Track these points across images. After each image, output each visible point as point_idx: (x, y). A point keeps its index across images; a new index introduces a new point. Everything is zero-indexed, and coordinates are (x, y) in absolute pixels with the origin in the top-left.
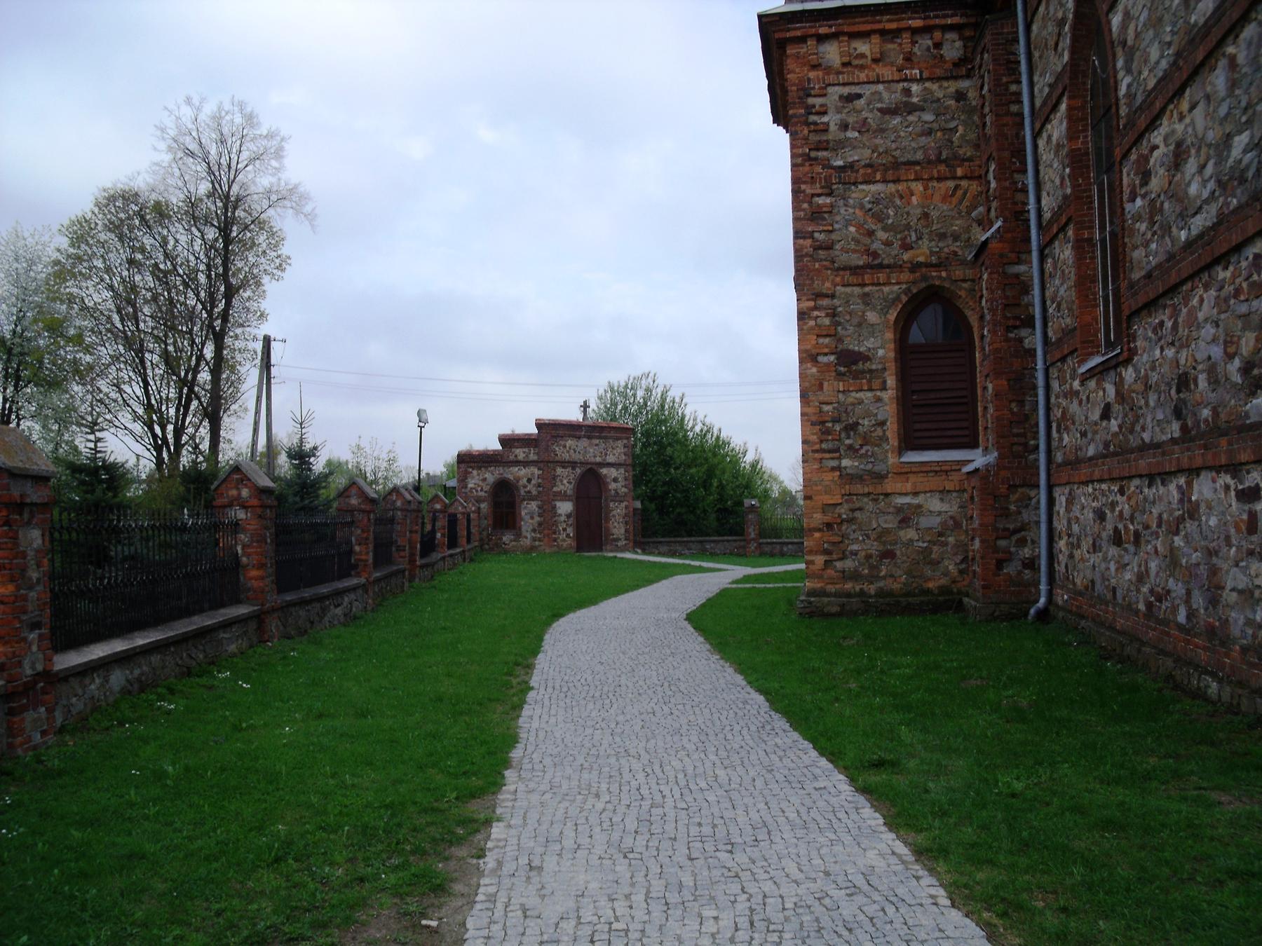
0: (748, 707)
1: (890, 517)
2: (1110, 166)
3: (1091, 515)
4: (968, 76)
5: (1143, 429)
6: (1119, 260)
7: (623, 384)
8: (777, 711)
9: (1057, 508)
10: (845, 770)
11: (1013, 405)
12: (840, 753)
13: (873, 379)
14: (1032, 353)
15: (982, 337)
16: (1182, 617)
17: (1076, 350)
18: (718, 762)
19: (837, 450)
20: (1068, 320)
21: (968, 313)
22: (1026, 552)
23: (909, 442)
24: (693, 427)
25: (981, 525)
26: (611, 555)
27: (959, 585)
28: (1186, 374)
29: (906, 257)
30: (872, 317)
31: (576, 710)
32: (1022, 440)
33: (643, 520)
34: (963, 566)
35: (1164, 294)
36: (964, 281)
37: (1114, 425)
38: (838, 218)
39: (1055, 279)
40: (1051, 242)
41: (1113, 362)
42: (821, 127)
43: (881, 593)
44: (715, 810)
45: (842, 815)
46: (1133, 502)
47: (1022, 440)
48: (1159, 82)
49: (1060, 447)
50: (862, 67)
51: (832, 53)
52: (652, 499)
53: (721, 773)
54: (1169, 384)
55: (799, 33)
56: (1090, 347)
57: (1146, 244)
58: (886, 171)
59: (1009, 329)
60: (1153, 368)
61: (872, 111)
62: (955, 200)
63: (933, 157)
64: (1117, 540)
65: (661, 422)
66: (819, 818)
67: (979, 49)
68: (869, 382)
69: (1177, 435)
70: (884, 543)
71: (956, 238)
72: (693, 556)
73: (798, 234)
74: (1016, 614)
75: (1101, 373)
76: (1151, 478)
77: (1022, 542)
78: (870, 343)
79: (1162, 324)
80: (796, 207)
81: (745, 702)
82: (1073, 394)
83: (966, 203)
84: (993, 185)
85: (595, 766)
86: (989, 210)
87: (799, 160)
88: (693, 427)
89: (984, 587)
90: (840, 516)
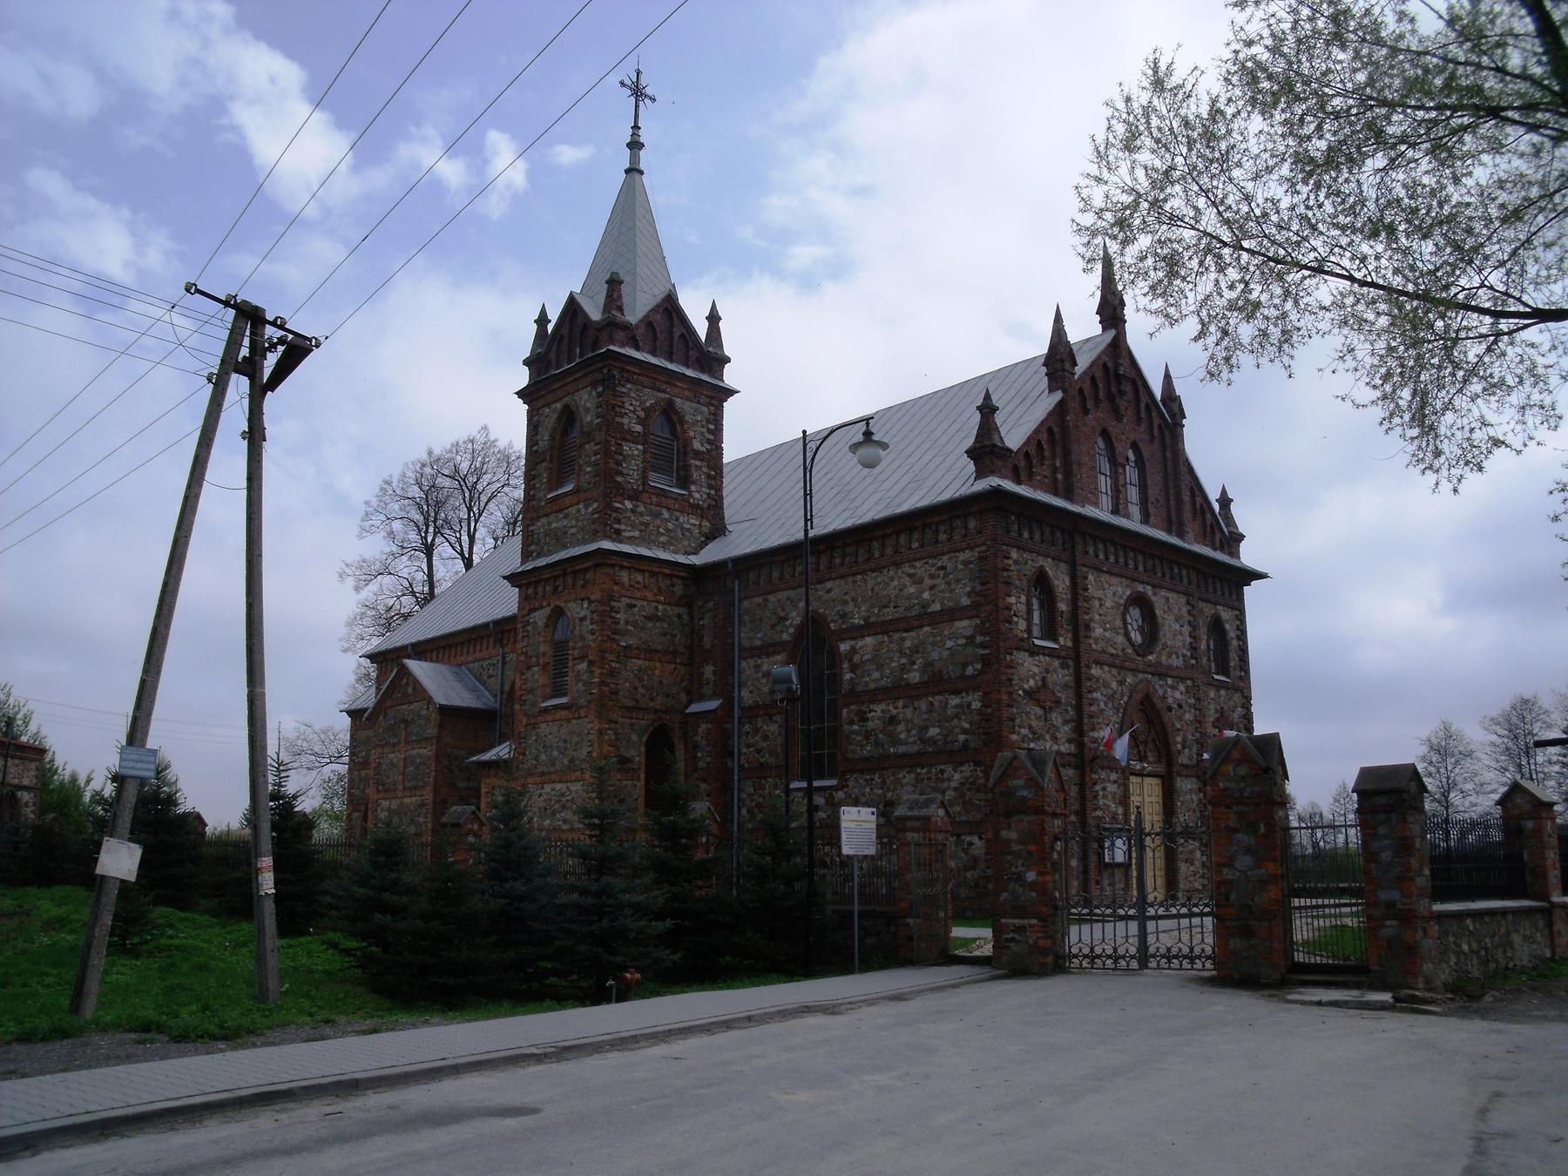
30: (634, 737)
51: (624, 576)
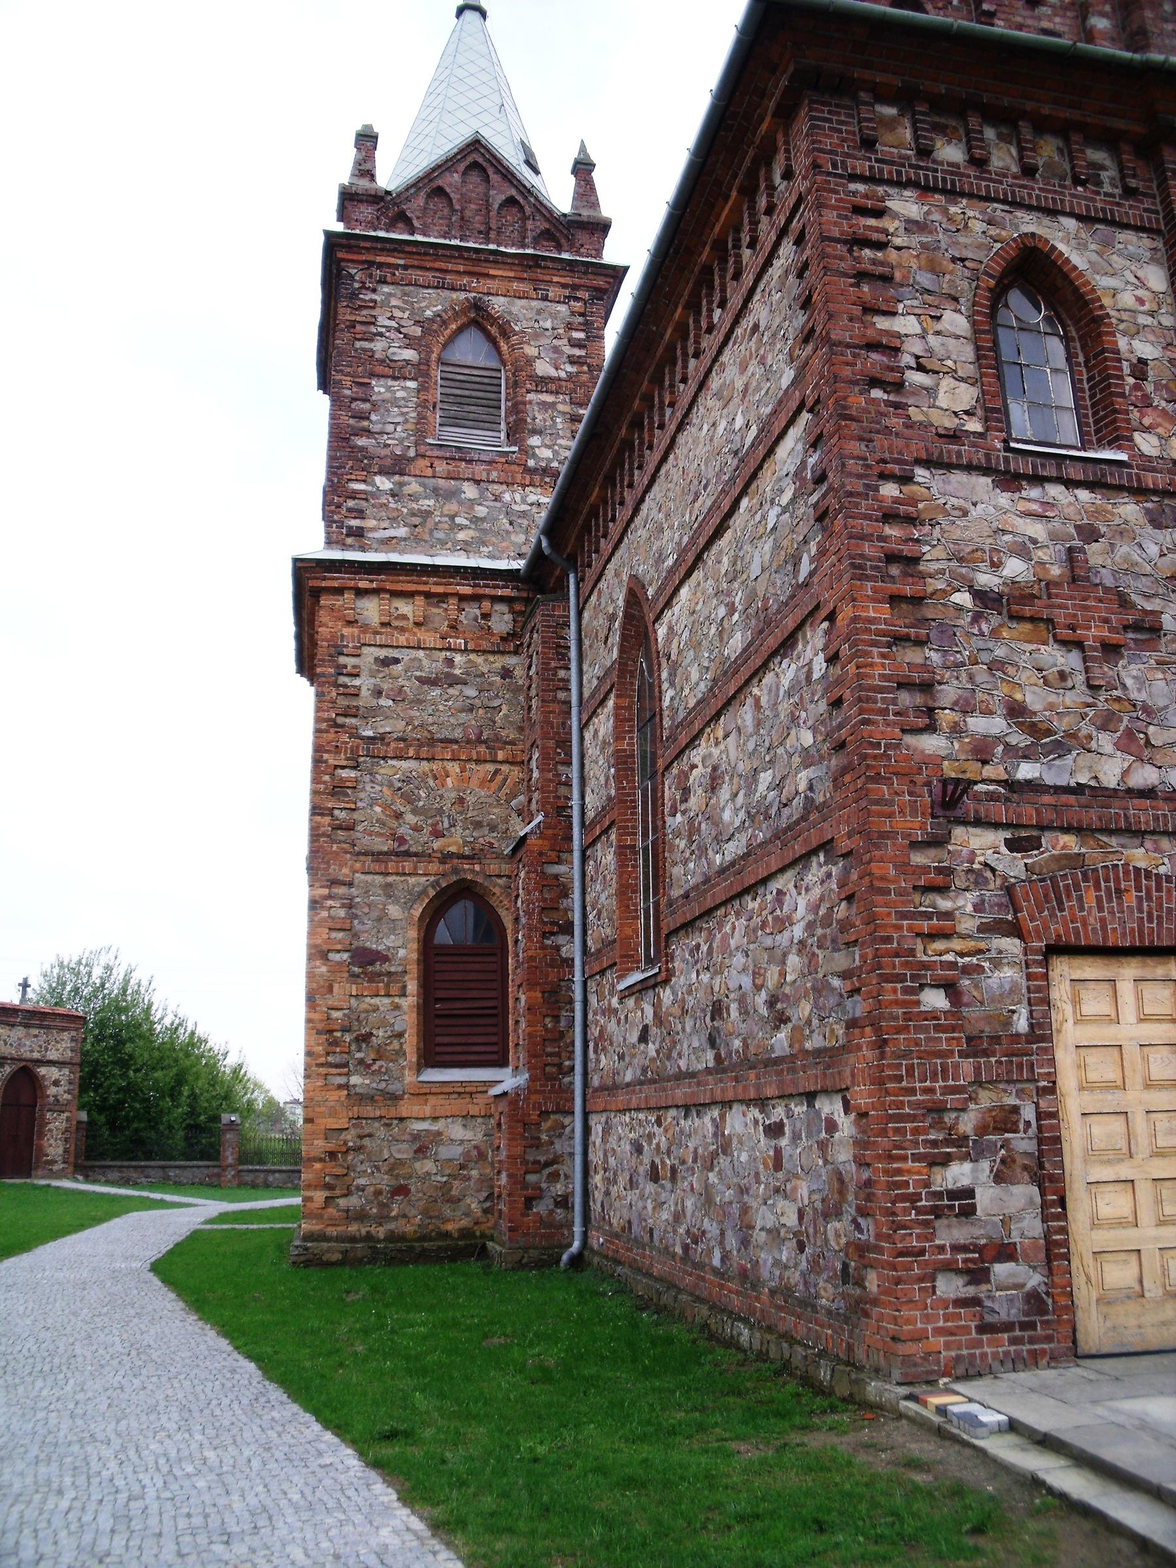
0: (237, 1377)
1: (405, 1146)
2: (654, 775)
3: (628, 1147)
4: (516, 652)
5: (680, 1055)
6: (659, 876)
7: (75, 959)
8: (271, 1380)
9: (592, 1138)
10: (353, 1443)
11: (548, 1020)
12: (347, 1424)
13: (391, 982)
14: (569, 962)
15: (516, 941)
16: (716, 1261)
17: (615, 964)
18: (206, 1442)
19: (346, 1065)
20: (608, 931)
21: (502, 913)
22: (559, 1188)
23: (430, 1057)
24: (162, 1019)
25: (508, 1157)
26: (43, 1182)
27: (483, 1227)
28: (720, 1001)
29: (437, 845)
30: (394, 911)
31: (21, 1389)
32: (556, 1060)
33: (87, 1137)
34: (488, 1204)
35: (701, 916)
36: (499, 876)
37: (652, 1049)
38: (362, 795)
39: (596, 885)
40: (593, 843)
41: (652, 982)
42: (352, 691)
43: (392, 1237)
44: (207, 1498)
45: (351, 1492)
46: (669, 1135)
47: (556, 1060)
48: (699, 703)
49: (598, 1069)
50: (402, 630)
51: (371, 610)
52: (101, 1109)
53: (210, 1455)
54: (704, 1011)
55: (336, 584)
56: (628, 962)
57: (685, 862)
58: (421, 746)
59: (544, 935)
60: (690, 992)
61: (409, 679)
62: (494, 785)
63: (473, 737)
64: (654, 1176)
65: (120, 1010)
66: (325, 1498)
67: (529, 627)
68: (387, 986)
69: (711, 1064)
70: (397, 1177)
71: (493, 828)
72: (151, 1187)
73: (316, 810)
74: (547, 1261)
75: (640, 991)
76: (687, 1109)
77: (554, 1177)
78: (390, 941)
79: (698, 946)
80: (316, 780)
81: (233, 1371)
82: (610, 1012)
83: (505, 790)
84: (536, 774)
85: (54, 1457)
86: (530, 801)
87: (324, 726)
88: (162, 1019)
89: (511, 1229)
90: (345, 1143)
